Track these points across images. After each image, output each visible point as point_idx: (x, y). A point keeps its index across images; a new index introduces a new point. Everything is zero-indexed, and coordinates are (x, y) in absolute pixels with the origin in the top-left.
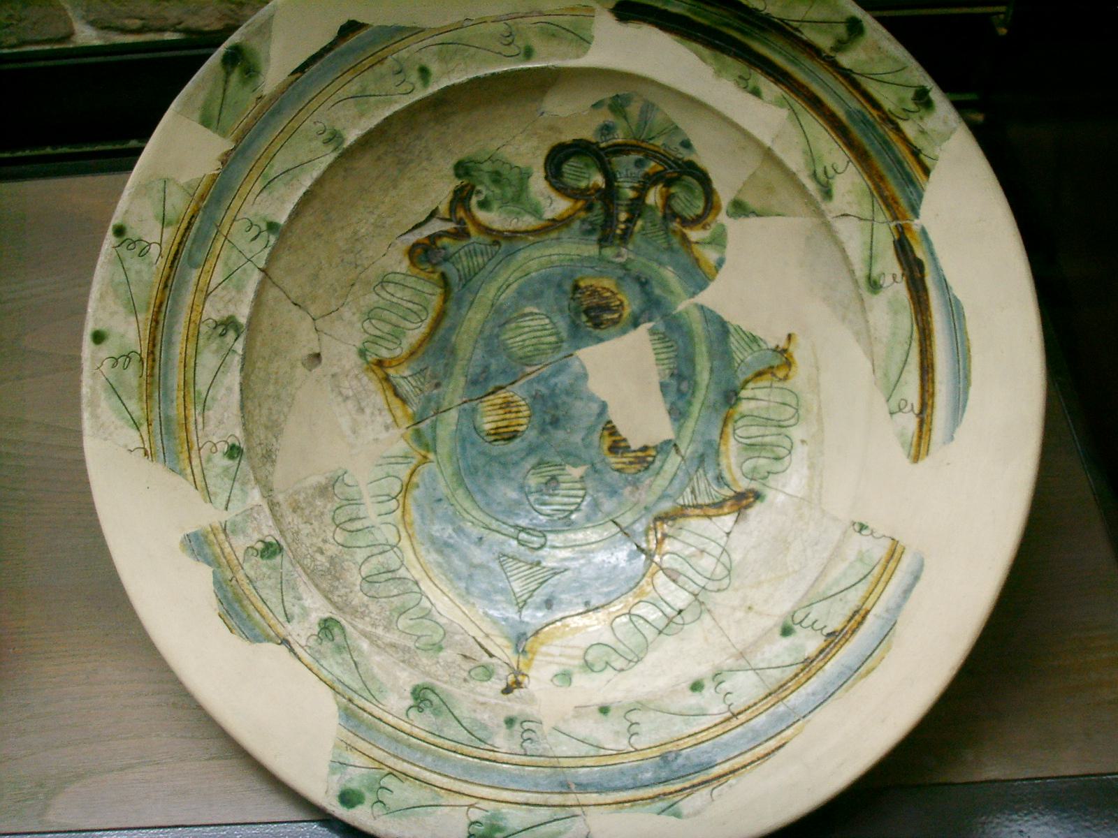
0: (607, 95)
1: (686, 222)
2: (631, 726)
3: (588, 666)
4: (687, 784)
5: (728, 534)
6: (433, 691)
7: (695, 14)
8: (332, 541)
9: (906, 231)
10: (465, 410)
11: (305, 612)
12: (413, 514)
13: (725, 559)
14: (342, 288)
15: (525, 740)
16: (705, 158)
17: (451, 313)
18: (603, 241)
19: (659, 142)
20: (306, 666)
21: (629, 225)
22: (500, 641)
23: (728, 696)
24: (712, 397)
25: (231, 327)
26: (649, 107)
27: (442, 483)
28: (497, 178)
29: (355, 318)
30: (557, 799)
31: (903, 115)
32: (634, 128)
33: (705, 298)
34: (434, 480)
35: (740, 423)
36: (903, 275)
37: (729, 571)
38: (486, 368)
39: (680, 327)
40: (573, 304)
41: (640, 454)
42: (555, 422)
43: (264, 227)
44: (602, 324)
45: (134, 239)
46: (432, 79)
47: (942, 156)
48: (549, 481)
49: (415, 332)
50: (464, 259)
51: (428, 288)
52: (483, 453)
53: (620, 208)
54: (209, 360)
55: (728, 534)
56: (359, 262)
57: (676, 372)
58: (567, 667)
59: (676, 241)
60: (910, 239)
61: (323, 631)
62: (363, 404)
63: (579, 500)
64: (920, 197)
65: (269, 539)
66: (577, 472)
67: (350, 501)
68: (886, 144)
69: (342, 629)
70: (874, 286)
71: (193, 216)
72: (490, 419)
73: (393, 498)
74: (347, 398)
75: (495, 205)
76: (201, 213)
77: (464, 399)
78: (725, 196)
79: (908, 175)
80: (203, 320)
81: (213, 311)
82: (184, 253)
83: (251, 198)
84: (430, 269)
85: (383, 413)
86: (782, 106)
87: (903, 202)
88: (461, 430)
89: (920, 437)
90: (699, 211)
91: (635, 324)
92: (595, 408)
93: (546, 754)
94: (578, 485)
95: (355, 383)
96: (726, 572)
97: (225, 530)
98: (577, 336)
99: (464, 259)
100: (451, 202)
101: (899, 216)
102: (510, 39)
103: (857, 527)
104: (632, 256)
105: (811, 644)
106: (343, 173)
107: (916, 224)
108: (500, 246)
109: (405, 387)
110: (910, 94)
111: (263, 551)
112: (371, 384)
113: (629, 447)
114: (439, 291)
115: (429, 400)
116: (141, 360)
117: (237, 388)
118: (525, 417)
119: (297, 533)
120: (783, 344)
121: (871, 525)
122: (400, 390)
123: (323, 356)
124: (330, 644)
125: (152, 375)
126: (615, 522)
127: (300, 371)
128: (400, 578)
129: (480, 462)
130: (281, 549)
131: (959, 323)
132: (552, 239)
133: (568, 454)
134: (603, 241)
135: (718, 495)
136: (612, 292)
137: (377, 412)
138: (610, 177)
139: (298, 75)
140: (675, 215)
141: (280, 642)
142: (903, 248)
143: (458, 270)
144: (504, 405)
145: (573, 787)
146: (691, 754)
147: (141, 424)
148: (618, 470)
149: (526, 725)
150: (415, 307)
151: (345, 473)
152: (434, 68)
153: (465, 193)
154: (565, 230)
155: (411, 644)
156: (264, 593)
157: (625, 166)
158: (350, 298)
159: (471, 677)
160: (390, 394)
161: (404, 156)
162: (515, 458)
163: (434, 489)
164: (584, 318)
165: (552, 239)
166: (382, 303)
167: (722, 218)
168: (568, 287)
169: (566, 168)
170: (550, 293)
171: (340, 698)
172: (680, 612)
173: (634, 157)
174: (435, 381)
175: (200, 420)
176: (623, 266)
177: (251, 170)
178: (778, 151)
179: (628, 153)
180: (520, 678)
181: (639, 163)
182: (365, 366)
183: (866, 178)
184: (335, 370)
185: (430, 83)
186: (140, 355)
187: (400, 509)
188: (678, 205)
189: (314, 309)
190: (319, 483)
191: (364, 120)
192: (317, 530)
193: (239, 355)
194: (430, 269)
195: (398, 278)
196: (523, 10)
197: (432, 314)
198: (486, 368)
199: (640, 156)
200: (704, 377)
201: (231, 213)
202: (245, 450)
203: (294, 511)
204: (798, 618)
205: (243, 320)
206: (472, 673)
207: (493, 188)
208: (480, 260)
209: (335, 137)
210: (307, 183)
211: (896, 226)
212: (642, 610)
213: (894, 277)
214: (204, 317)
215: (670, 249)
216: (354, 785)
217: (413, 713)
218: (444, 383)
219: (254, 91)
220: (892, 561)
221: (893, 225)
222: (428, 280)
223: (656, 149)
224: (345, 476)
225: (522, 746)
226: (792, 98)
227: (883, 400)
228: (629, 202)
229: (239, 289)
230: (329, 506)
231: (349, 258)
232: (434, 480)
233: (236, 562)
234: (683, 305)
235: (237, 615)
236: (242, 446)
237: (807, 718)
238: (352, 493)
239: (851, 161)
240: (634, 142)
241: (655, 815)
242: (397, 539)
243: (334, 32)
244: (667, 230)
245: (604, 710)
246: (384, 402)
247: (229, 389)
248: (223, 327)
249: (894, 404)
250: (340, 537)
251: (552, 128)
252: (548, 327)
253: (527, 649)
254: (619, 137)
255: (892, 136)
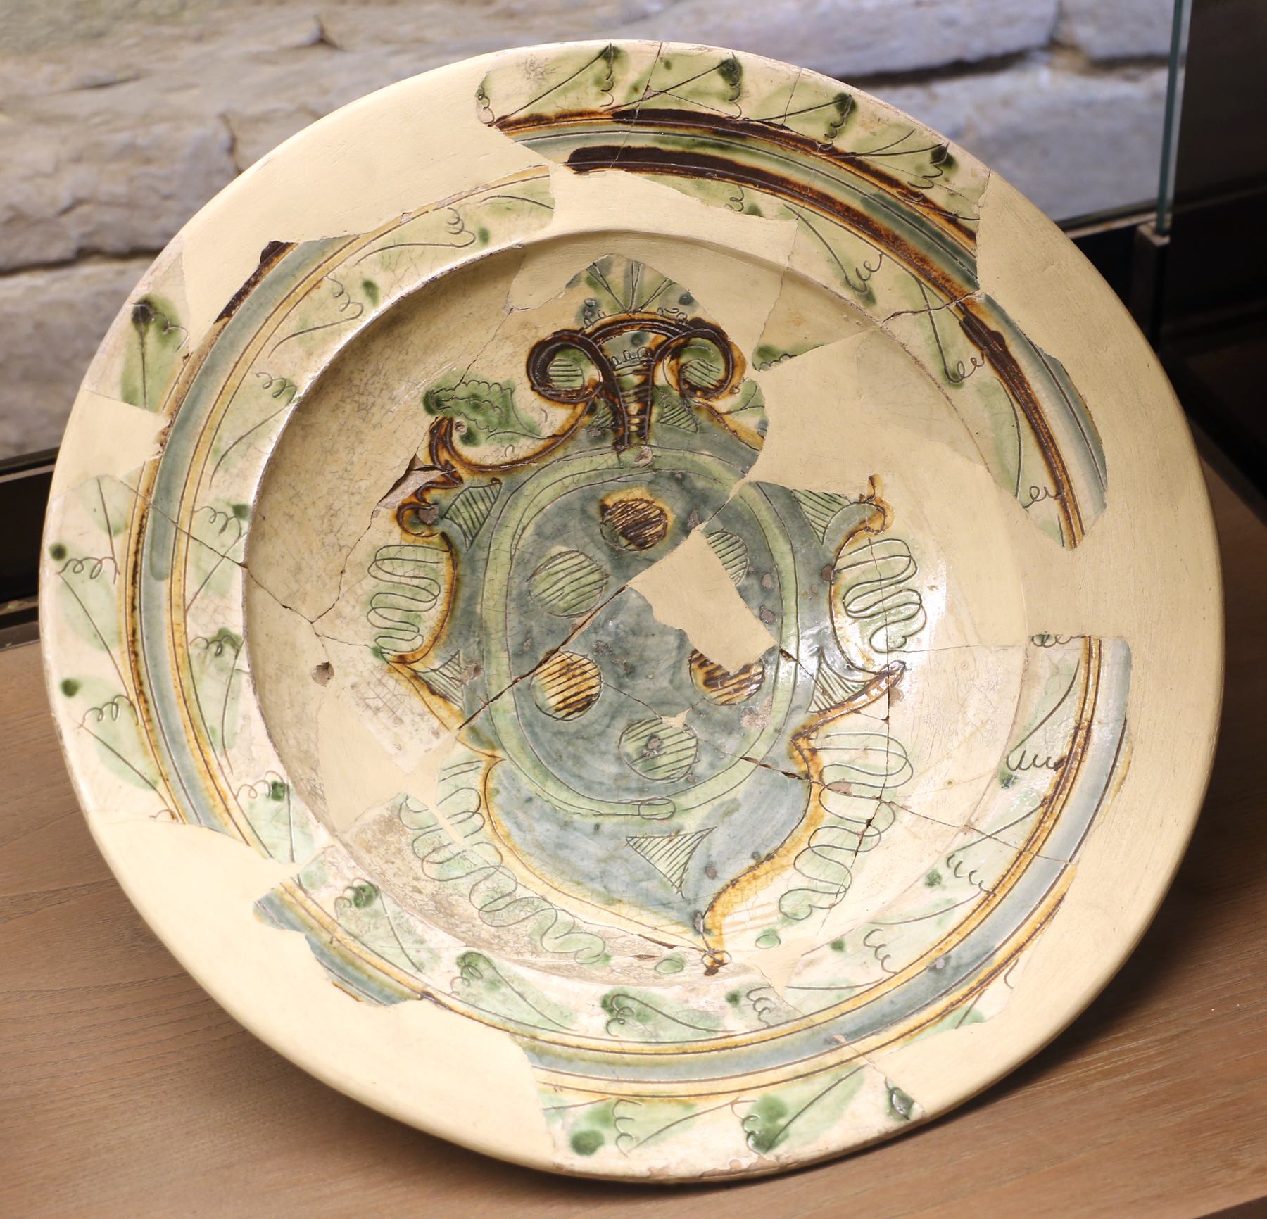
0: (581, 265)
1: (706, 393)
2: (876, 951)
3: (790, 918)
4: (973, 984)
5: (887, 720)
6: (627, 996)
7: (662, 142)
8: (424, 877)
9: (969, 307)
10: (519, 690)
11: (435, 955)
12: (506, 825)
13: (894, 747)
14: (331, 578)
15: (760, 1013)
16: (709, 310)
17: (466, 580)
18: (620, 444)
19: (653, 307)
20: (463, 1014)
21: (643, 417)
22: (673, 929)
23: (973, 875)
24: (803, 579)
25: (226, 642)
26: (634, 268)
27: (525, 779)
28: (476, 402)
29: (358, 611)
30: (831, 1059)
31: (925, 183)
32: (620, 299)
33: (755, 474)
34: (514, 780)
35: (849, 597)
36: (982, 355)
37: (906, 758)
38: (528, 633)
39: (739, 516)
40: (605, 529)
41: (743, 677)
42: (631, 671)
43: (230, 513)
44: (647, 542)
45: (80, 559)
46: (381, 295)
47: (983, 213)
48: (649, 740)
49: (432, 614)
50: (463, 510)
51: (431, 556)
52: (559, 733)
53: (627, 399)
54: (210, 689)
55: (887, 720)
56: (342, 543)
57: (751, 569)
58: (766, 928)
59: (703, 418)
60: (977, 315)
61: (466, 970)
62: (399, 713)
63: (692, 751)
64: (974, 265)
65: (356, 884)
66: (677, 721)
67: (426, 829)
68: (918, 222)
69: (488, 961)
70: (954, 378)
71: (143, 517)
72: (554, 691)
73: (474, 813)
74: (378, 709)
75: (482, 436)
76: (151, 510)
77: (514, 678)
78: (745, 346)
79: (952, 246)
80: (190, 641)
81: (200, 627)
82: (144, 564)
83: (206, 480)
84: (427, 533)
85: (426, 718)
86: (788, 218)
87: (957, 280)
88: (523, 714)
89: (1068, 519)
90: (721, 375)
91: (687, 532)
92: (672, 641)
93: (792, 1018)
94: (686, 736)
95: (379, 690)
96: (905, 761)
97: (300, 886)
98: (623, 566)
99: (463, 510)
100: (430, 446)
101: (956, 294)
102: (459, 226)
103: (1037, 641)
104: (657, 453)
105: (1043, 781)
106: (301, 433)
107: (978, 297)
108: (501, 484)
109: (440, 682)
110: (927, 156)
111: (356, 899)
112: (397, 685)
113: (728, 673)
114: (445, 555)
115: (472, 690)
116: (131, 704)
117: (256, 715)
118: (594, 677)
119: (383, 874)
120: (867, 491)
121: (1052, 633)
122: (435, 686)
123: (334, 664)
124: (480, 983)
125: (150, 720)
126: (746, 759)
127: (314, 688)
128: (521, 900)
129: (560, 745)
130: (376, 890)
131: (1064, 382)
132: (559, 460)
133: (663, 703)
134: (620, 444)
135: (856, 684)
136: (647, 501)
137: (418, 719)
138: (605, 366)
139: (225, 319)
140: (694, 389)
141: (419, 996)
142: (973, 328)
143: (460, 526)
144: (564, 671)
145: (842, 1040)
146: (962, 953)
147: (156, 782)
148: (724, 703)
149: (754, 997)
150: (424, 583)
151: (407, 798)
152: (380, 280)
153: (443, 431)
154: (571, 444)
155: (572, 962)
156: (377, 946)
157: (619, 347)
158: (344, 588)
159: (660, 973)
160: (426, 693)
161: (363, 399)
162: (599, 728)
163: (519, 790)
164: (624, 542)
165: (559, 460)
166: (383, 587)
167: (750, 373)
168: (594, 510)
169: (552, 370)
170: (574, 523)
171: (519, 1038)
172: (869, 823)
173: (628, 334)
174: (474, 665)
175: (224, 762)
176: (650, 467)
177: (197, 447)
178: (799, 268)
179: (620, 331)
180: (718, 957)
181: (636, 340)
182: (386, 667)
183: (906, 266)
184: (352, 679)
185: (381, 298)
186: (128, 698)
187: (488, 823)
188: (694, 377)
189: (308, 610)
190: (381, 816)
191: (314, 358)
192: (402, 868)
193: (247, 673)
194: (427, 533)
195: (392, 552)
196: (467, 189)
197: (445, 587)
198: (528, 633)
199: (636, 331)
200: (785, 561)
201: (188, 502)
202: (291, 785)
203: (369, 852)
204: (1014, 762)
205: (237, 629)
206: (659, 969)
207: (472, 416)
208: (482, 507)
209: (286, 387)
210: (268, 448)
211: (957, 305)
212: (823, 837)
213: (974, 361)
214: (191, 638)
215: (700, 429)
216: (585, 1127)
217: (615, 1028)
218: (484, 666)
219: (178, 349)
220: (1092, 660)
221: (952, 307)
222: (429, 547)
223: (653, 317)
224: (408, 801)
225: (759, 1019)
226: (796, 205)
227: (1011, 496)
228: (637, 390)
229: (223, 595)
230: (403, 840)
231: (331, 538)
232: (514, 780)
233: (329, 919)
234: (735, 489)
235: (356, 980)
236: (285, 782)
237: (1074, 861)
238: (424, 818)
239: (883, 253)
240: (624, 316)
241: (954, 1030)
242: (499, 857)
243: (257, 262)
244: (689, 410)
245: (838, 946)
246: (421, 704)
247: (246, 717)
248: (218, 644)
249: (1024, 496)
250: (432, 871)
251: (524, 325)
252: (585, 564)
253: (708, 926)
254: (607, 314)
255: (921, 210)
